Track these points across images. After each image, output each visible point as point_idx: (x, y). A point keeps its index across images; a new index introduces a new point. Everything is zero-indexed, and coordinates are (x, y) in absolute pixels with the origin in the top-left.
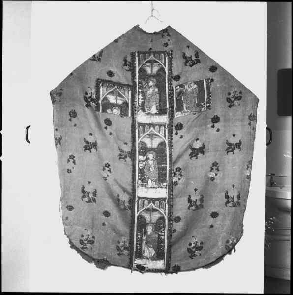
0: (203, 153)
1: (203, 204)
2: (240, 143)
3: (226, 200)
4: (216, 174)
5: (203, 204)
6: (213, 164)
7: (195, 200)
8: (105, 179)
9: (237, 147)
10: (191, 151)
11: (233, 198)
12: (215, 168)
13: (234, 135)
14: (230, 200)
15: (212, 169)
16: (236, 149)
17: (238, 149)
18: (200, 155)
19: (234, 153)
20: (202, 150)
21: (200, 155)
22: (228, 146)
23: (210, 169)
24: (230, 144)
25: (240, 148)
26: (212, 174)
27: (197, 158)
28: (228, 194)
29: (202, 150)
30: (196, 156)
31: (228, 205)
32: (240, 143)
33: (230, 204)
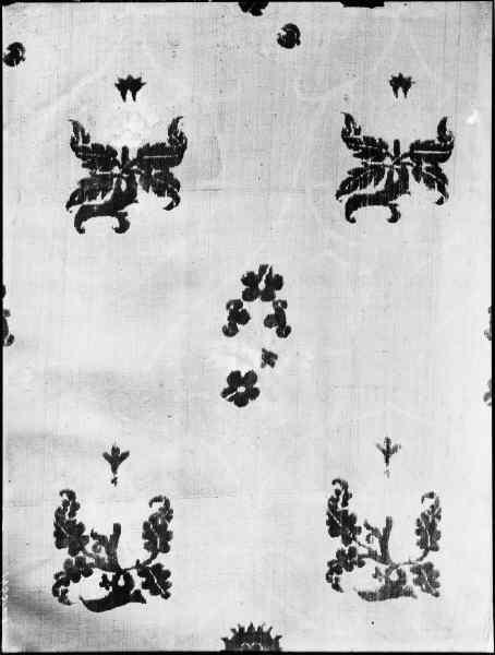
0: (168, 188)
1: (161, 559)
2: (174, 147)
3: (64, 554)
4: (269, 358)
5: (161, 559)
6: (250, 280)
7: (108, 532)
8: (191, 281)
9: (417, 174)
10: (85, 173)
11: (110, 543)
12: (259, 309)
13: (401, 83)
14: (362, 543)
15: (238, 317)
16: (141, 193)
17: (429, 183)
18: (148, 204)
19: (395, 218)
20: (159, 166)
21: (148, 204)
22: (358, 163)
23: (223, 319)
24: (371, 149)
25: (438, 181)
26: (243, 352)
27: (123, 227)
28: (79, 518)
29: (159, 166)
30: (117, 208)
31: (345, 577)
32: (174, 147)
33: (362, 578)
